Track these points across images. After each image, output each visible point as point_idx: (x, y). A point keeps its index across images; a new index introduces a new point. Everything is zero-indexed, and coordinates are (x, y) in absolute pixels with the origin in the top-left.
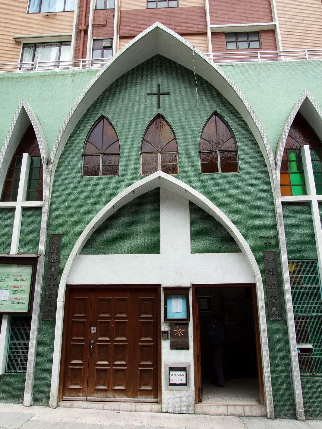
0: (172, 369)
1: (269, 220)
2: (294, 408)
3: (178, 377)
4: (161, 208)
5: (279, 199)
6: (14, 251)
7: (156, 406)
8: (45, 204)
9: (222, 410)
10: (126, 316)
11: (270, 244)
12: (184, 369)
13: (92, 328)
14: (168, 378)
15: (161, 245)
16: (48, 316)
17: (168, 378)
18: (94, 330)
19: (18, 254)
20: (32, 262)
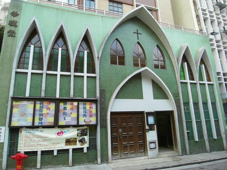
0: (151, 143)
1: (176, 88)
2: (186, 151)
3: (153, 146)
4: (142, 81)
5: (179, 81)
6: (27, 95)
7: (146, 157)
8: (97, 75)
9: (167, 155)
10: (132, 124)
11: (177, 97)
12: (154, 143)
13: (120, 129)
14: (150, 147)
15: (143, 95)
16: (104, 126)
17: (150, 147)
18: (120, 130)
19: (29, 97)
20: (95, 101)
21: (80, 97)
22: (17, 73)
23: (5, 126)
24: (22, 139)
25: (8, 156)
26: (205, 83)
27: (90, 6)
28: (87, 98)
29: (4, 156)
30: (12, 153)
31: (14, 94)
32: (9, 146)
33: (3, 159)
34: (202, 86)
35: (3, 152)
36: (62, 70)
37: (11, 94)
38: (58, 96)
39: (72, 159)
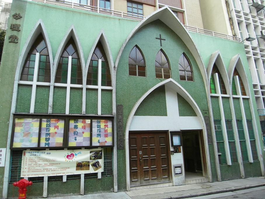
0: (176, 167)
1: (205, 103)
2: (217, 177)
3: (178, 170)
4: (166, 95)
5: (209, 95)
6: (32, 111)
7: (171, 184)
8: (113, 88)
9: (195, 182)
10: (154, 145)
11: (206, 113)
12: (180, 167)
13: (140, 152)
14: (175, 172)
15: (167, 112)
16: (121, 148)
17: (175, 172)
18: (140, 153)
19: (34, 113)
20: (111, 119)
21: (93, 113)
22: (19, 85)
23: (6, 147)
24: (26, 163)
25: (10, 182)
26: (240, 98)
27: (105, 8)
28: (101, 114)
29: (4, 183)
30: (14, 179)
31: (16, 110)
32: (10, 171)
33: (4, 186)
34: (236, 101)
35: (3, 178)
36: (72, 82)
37: (13, 110)
38: (67, 113)
39: (84, 186)
